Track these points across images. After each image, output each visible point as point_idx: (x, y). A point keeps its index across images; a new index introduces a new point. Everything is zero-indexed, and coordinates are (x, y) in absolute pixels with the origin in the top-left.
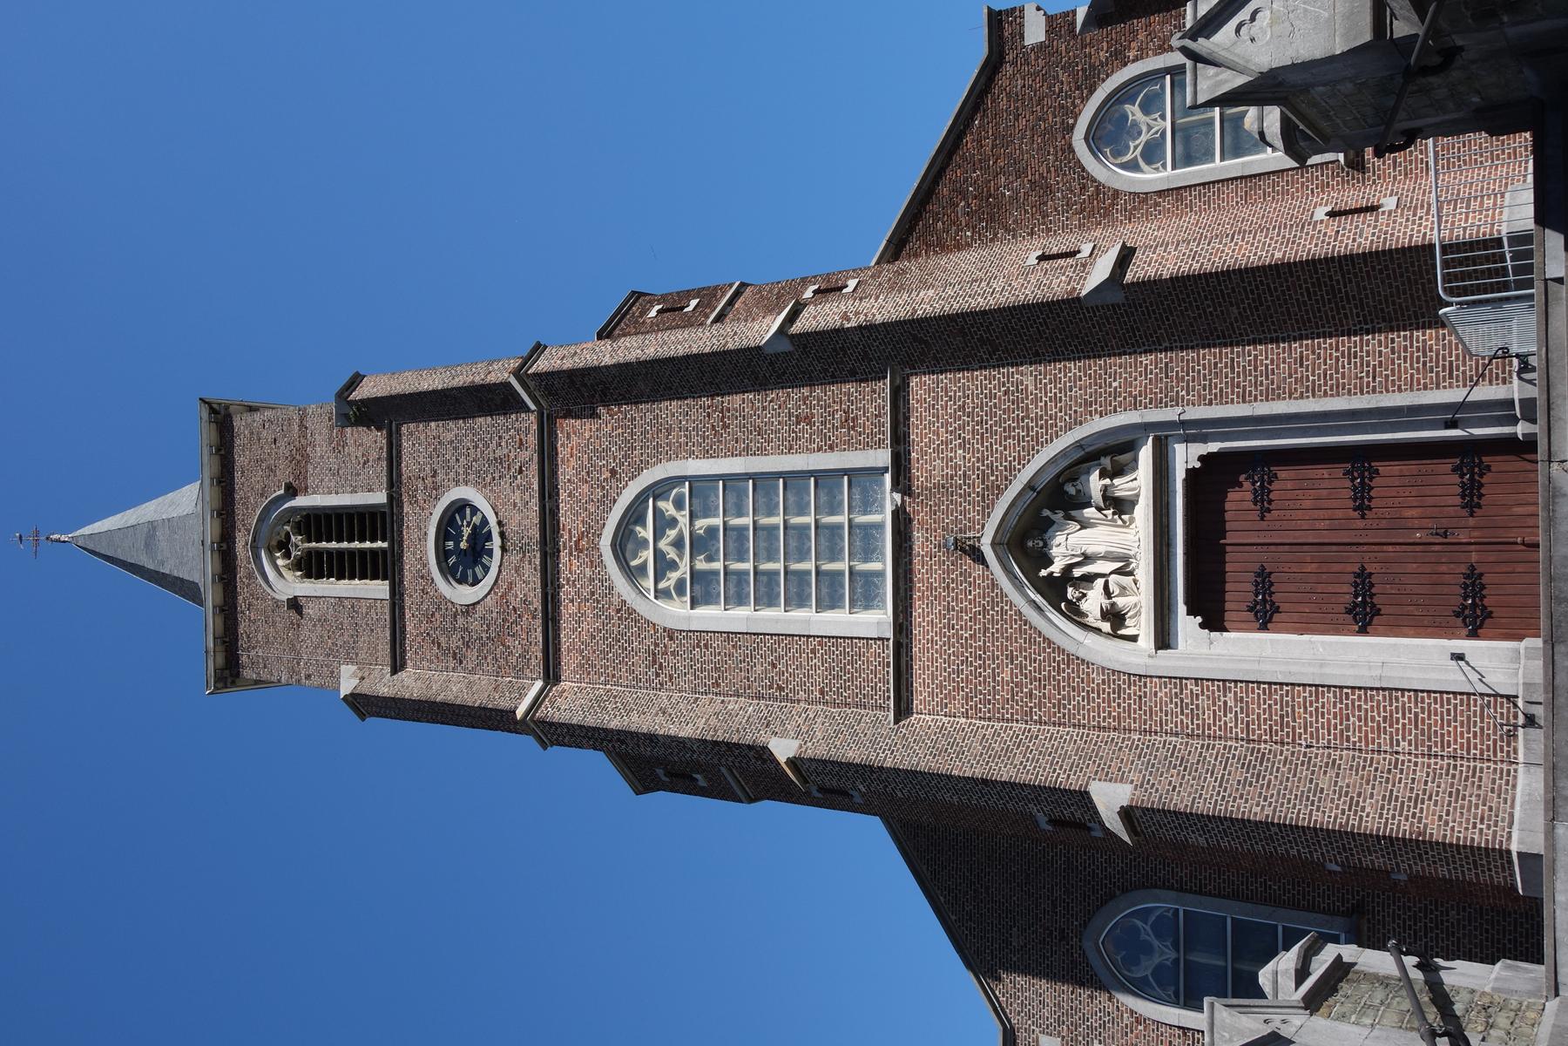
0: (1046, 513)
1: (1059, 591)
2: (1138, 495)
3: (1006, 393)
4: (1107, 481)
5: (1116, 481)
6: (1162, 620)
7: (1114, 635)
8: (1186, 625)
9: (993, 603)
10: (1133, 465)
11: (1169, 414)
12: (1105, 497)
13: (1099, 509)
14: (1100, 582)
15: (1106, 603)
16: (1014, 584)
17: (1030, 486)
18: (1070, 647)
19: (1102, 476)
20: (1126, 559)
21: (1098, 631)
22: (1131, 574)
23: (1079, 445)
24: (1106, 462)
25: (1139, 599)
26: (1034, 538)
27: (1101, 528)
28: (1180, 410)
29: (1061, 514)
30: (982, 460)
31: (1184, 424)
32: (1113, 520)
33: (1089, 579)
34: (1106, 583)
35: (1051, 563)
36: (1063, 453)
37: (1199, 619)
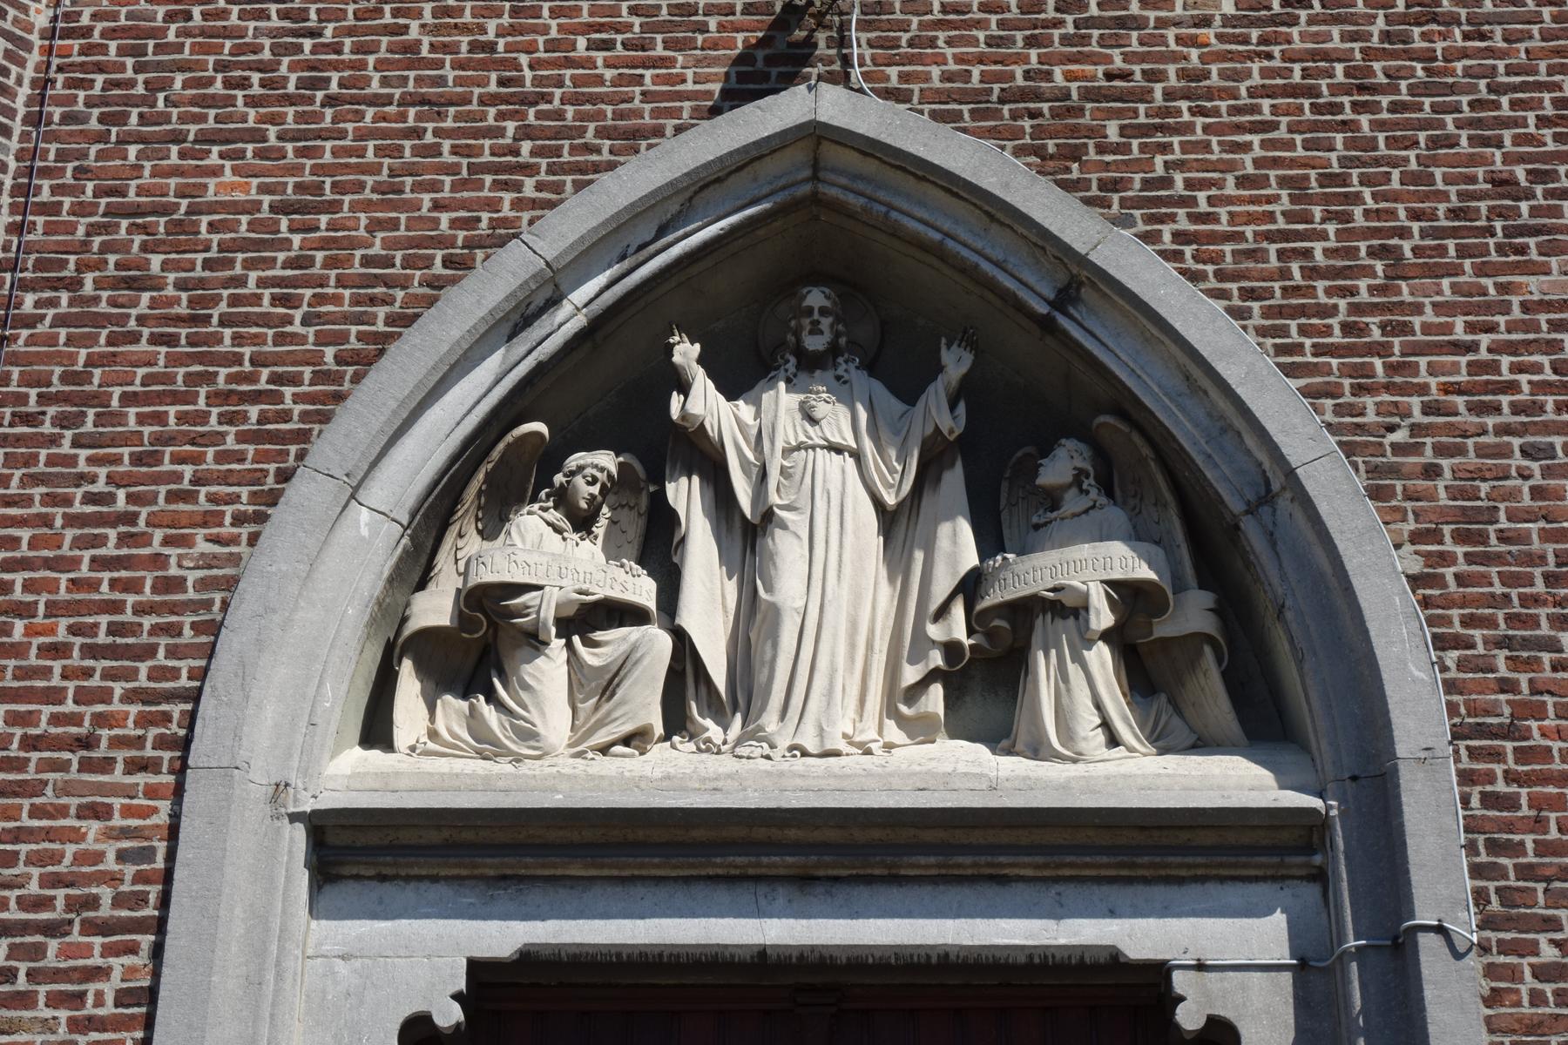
0: (956, 364)
1: (599, 418)
2: (1038, 750)
3: (1503, 184)
4: (1103, 617)
5: (1101, 657)
6: (449, 849)
7: (398, 647)
8: (430, 953)
9: (548, 137)
10: (1175, 731)
11: (1440, 886)
12: (1026, 611)
13: (970, 586)
14: (642, 589)
15: (545, 607)
16: (672, 190)
17: (1080, 280)
18: (339, 444)
19: (1125, 593)
20: (743, 696)
21: (415, 571)
22: (676, 722)
23: (1278, 486)
24: (1193, 614)
25: (553, 747)
26: (842, 313)
27: (886, 596)
28: (1466, 928)
29: (950, 423)
30: (1193, 85)
31: (1395, 950)
32: (922, 642)
33: (659, 547)
34: (628, 614)
35: (732, 389)
36: (1235, 420)
37: (449, 1015)
